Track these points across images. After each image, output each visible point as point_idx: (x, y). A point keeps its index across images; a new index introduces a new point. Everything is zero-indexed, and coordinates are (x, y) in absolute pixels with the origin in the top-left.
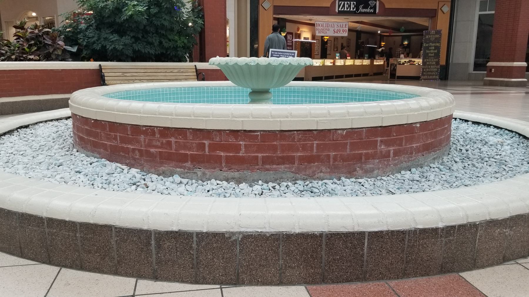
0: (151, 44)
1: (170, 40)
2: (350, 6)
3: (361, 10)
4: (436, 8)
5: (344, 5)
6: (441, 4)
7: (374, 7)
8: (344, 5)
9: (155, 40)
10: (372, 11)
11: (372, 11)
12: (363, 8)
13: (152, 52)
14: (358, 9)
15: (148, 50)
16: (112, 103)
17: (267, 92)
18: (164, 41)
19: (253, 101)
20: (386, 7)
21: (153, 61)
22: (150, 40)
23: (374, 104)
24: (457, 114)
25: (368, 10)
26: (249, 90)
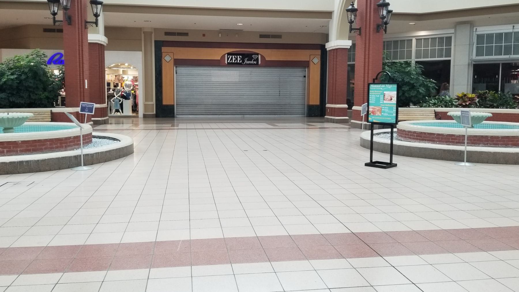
0: (22, 97)
1: (36, 95)
2: (237, 59)
3: (246, 62)
4: (309, 60)
5: (232, 59)
6: (312, 57)
7: (257, 59)
8: (232, 59)
9: (25, 95)
10: (255, 62)
11: (255, 62)
12: (248, 60)
13: (23, 102)
14: (243, 61)
15: (19, 101)
16: (412, 126)
17: (12, 128)
18: (32, 95)
19: (5, 133)
20: (267, 59)
21: (26, 107)
22: (22, 94)
23: (56, 131)
24: (94, 134)
25: (252, 62)
26: (3, 128)
